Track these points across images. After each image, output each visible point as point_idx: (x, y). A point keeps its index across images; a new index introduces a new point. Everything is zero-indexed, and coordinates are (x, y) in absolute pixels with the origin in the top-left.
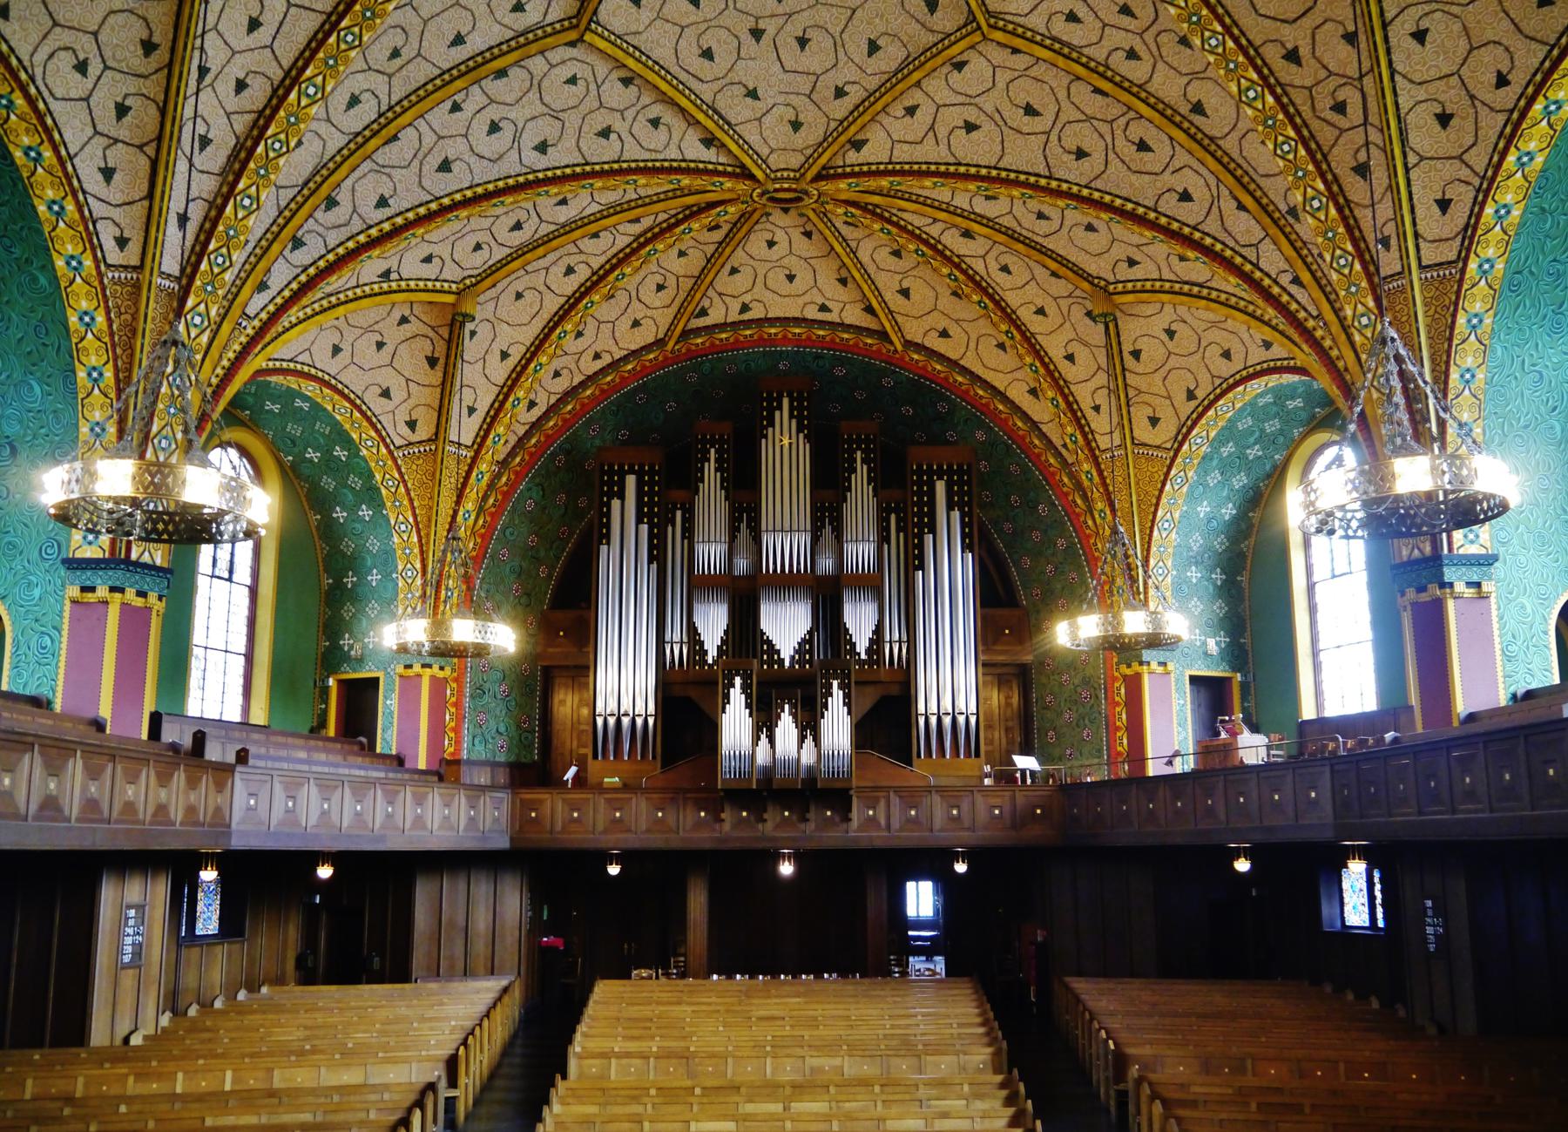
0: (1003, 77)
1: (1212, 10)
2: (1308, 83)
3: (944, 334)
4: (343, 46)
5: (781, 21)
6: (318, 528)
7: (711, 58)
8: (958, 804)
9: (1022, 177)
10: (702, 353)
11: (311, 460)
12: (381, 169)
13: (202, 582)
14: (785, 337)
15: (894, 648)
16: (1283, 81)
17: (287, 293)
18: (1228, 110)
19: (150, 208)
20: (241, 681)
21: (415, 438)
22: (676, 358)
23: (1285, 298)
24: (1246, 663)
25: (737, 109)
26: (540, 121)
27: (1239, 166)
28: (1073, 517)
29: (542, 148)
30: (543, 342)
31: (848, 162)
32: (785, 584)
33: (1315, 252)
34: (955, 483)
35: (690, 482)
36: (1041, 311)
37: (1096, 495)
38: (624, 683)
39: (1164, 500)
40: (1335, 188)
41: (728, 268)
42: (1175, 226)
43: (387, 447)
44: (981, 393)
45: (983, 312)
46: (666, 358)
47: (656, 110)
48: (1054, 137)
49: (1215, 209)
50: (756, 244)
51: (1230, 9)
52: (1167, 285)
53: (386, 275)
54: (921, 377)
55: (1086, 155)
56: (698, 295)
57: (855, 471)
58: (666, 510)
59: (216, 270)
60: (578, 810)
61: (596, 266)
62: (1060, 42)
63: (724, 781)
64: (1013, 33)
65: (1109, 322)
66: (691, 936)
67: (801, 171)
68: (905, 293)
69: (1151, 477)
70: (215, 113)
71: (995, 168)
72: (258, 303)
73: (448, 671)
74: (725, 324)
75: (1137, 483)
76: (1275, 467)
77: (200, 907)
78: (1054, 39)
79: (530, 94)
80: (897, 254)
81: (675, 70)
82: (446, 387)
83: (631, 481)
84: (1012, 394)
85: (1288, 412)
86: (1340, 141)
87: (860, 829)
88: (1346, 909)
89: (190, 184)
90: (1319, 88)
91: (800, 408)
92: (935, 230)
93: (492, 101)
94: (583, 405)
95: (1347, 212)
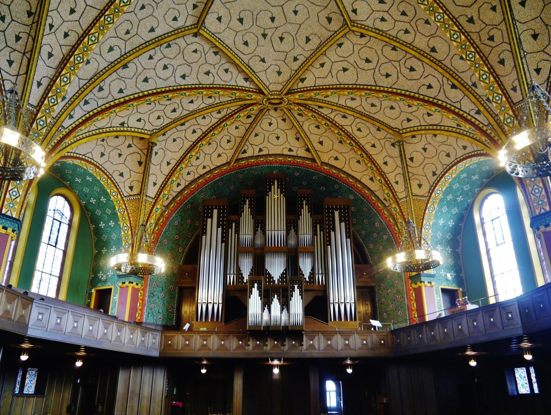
0: (357, 48)
1: (438, 4)
2: (478, 31)
3: (336, 159)
4: (106, 22)
5: (273, 30)
6: (93, 231)
7: (247, 45)
8: (348, 343)
9: (365, 87)
10: (245, 167)
11: (92, 203)
12: (121, 78)
13: (43, 247)
14: (276, 161)
15: (319, 277)
16: (467, 31)
17: (80, 121)
18: (445, 48)
19: (26, 78)
20: (56, 287)
21: (132, 193)
22: (234, 169)
23: (473, 120)
24: (463, 284)
25: (257, 66)
26: (183, 66)
27: (451, 70)
28: (389, 226)
29: (184, 77)
30: (183, 159)
31: (299, 87)
32: (276, 251)
33: (485, 99)
34: (342, 213)
35: (238, 212)
36: (373, 146)
37: (398, 216)
38: (210, 294)
39: (426, 217)
40: (492, 70)
41: (253, 134)
42: (426, 98)
43: (121, 195)
44: (351, 180)
45: (351, 147)
46: (230, 169)
47: (227, 66)
48: (377, 70)
49: (442, 90)
50: (264, 123)
51: (445, 4)
52: (423, 127)
53: (122, 124)
54: (327, 175)
55: (390, 75)
56: (243, 144)
57: (303, 208)
58: (230, 221)
59: (51, 104)
60: (189, 340)
61: (204, 131)
62: (379, 30)
63: (250, 326)
64: (361, 28)
65: (400, 144)
66: (235, 393)
67: (281, 91)
68: (321, 143)
69: (420, 208)
70: (53, 44)
71: (355, 85)
72: (68, 123)
73: (140, 286)
74: (253, 156)
75: (415, 211)
76: (468, 205)
77: (27, 381)
78: (376, 29)
79: (179, 55)
80: (318, 127)
81: (234, 49)
82: (145, 174)
83: (215, 212)
84: (363, 181)
85: (473, 182)
86: (492, 52)
87: (307, 349)
88: (518, 386)
89: (43, 70)
90: (482, 32)
91: (282, 185)
92: (332, 116)
93: (165, 57)
94: (198, 185)
95: (497, 79)
